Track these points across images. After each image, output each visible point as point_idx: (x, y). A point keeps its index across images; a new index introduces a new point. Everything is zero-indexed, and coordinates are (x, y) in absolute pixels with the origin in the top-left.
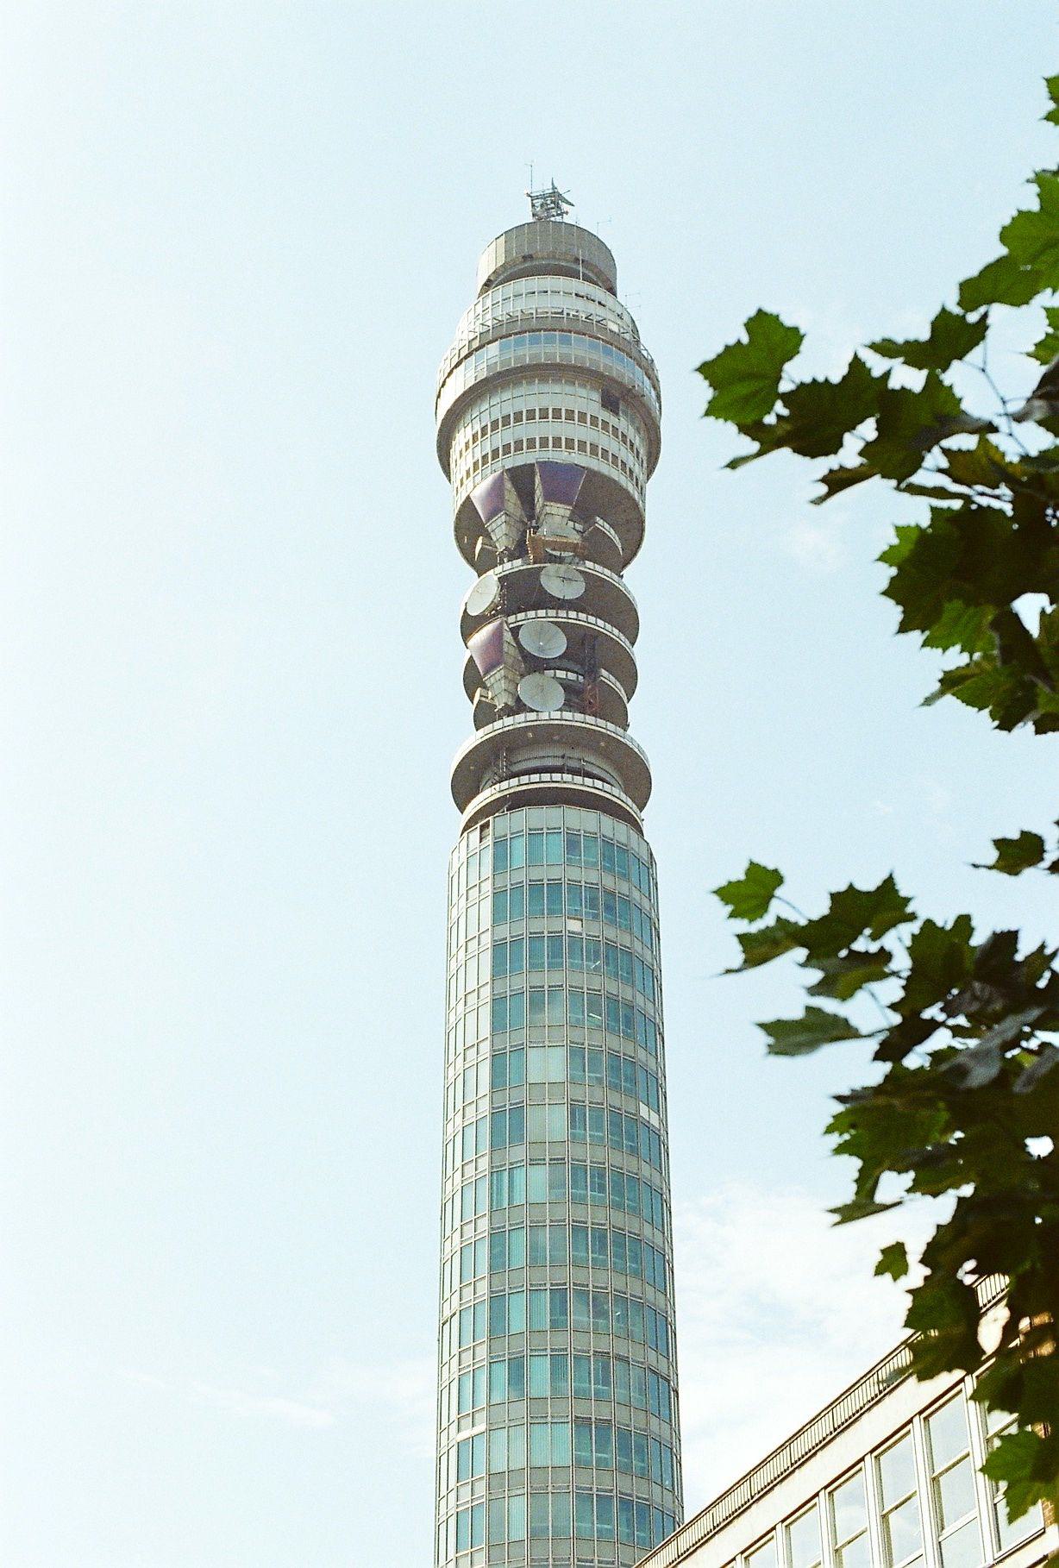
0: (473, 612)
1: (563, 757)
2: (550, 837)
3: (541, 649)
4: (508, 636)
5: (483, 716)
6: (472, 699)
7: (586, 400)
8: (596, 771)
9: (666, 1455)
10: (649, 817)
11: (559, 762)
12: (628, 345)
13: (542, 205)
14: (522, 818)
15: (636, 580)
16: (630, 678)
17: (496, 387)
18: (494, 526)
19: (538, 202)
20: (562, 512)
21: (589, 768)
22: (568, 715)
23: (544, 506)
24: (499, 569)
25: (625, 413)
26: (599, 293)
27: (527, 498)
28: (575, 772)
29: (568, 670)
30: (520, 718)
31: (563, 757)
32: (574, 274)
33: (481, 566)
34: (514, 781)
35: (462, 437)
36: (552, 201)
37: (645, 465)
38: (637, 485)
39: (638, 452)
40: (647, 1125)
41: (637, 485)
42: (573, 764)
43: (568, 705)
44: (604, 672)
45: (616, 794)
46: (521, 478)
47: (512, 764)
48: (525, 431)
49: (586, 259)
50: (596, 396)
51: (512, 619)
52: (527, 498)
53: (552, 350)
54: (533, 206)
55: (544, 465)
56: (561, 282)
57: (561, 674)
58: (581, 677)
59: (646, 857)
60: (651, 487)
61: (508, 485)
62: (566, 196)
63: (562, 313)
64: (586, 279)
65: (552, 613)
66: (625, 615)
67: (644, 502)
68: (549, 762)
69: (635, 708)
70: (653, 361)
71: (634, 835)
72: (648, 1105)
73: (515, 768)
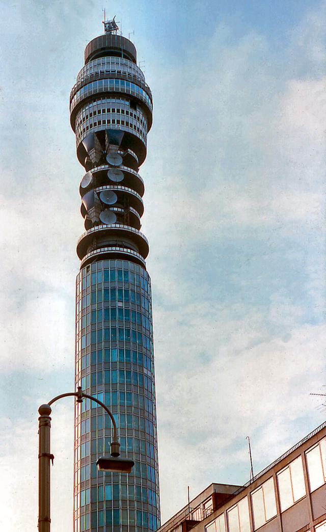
0: (84, 187)
1: (116, 241)
2: (113, 350)
3: (108, 201)
4: (96, 196)
5: (88, 225)
6: (84, 218)
7: (125, 104)
8: (129, 246)
9: (153, 470)
10: (148, 261)
11: (115, 243)
12: (138, 81)
13: (109, 26)
14: (102, 264)
15: (143, 172)
16: (141, 210)
17: (87, 103)
18: (91, 153)
19: (107, 25)
20: (115, 148)
21: (126, 245)
22: (118, 226)
23: (109, 146)
24: (93, 170)
25: (139, 108)
26: (129, 62)
27: (102, 142)
28: (120, 246)
29: (118, 207)
30: (100, 227)
31: (116, 241)
32: (119, 55)
33: (88, 167)
34: (99, 250)
35: (81, 116)
36: (111, 26)
37: (146, 128)
38: (141, 133)
39: (144, 123)
40: (147, 376)
41: (141, 133)
42: (120, 243)
43: (118, 222)
44: (131, 208)
45: (136, 254)
46: (101, 135)
47: (97, 243)
48: (101, 117)
49: (125, 49)
50: (128, 103)
51: (97, 189)
52: (102, 142)
53: (95, 87)
54: (105, 26)
55: (110, 130)
56: (115, 59)
57: (116, 209)
58: (123, 210)
59: (146, 276)
60: (149, 135)
61: (96, 138)
62: (54, 460)
63: (115, 72)
64: (125, 57)
65: (112, 187)
66: (138, 186)
67: (146, 142)
68: (111, 243)
69: (143, 220)
70: (149, 88)
71: (142, 269)
72: (147, 369)
73: (100, 245)
